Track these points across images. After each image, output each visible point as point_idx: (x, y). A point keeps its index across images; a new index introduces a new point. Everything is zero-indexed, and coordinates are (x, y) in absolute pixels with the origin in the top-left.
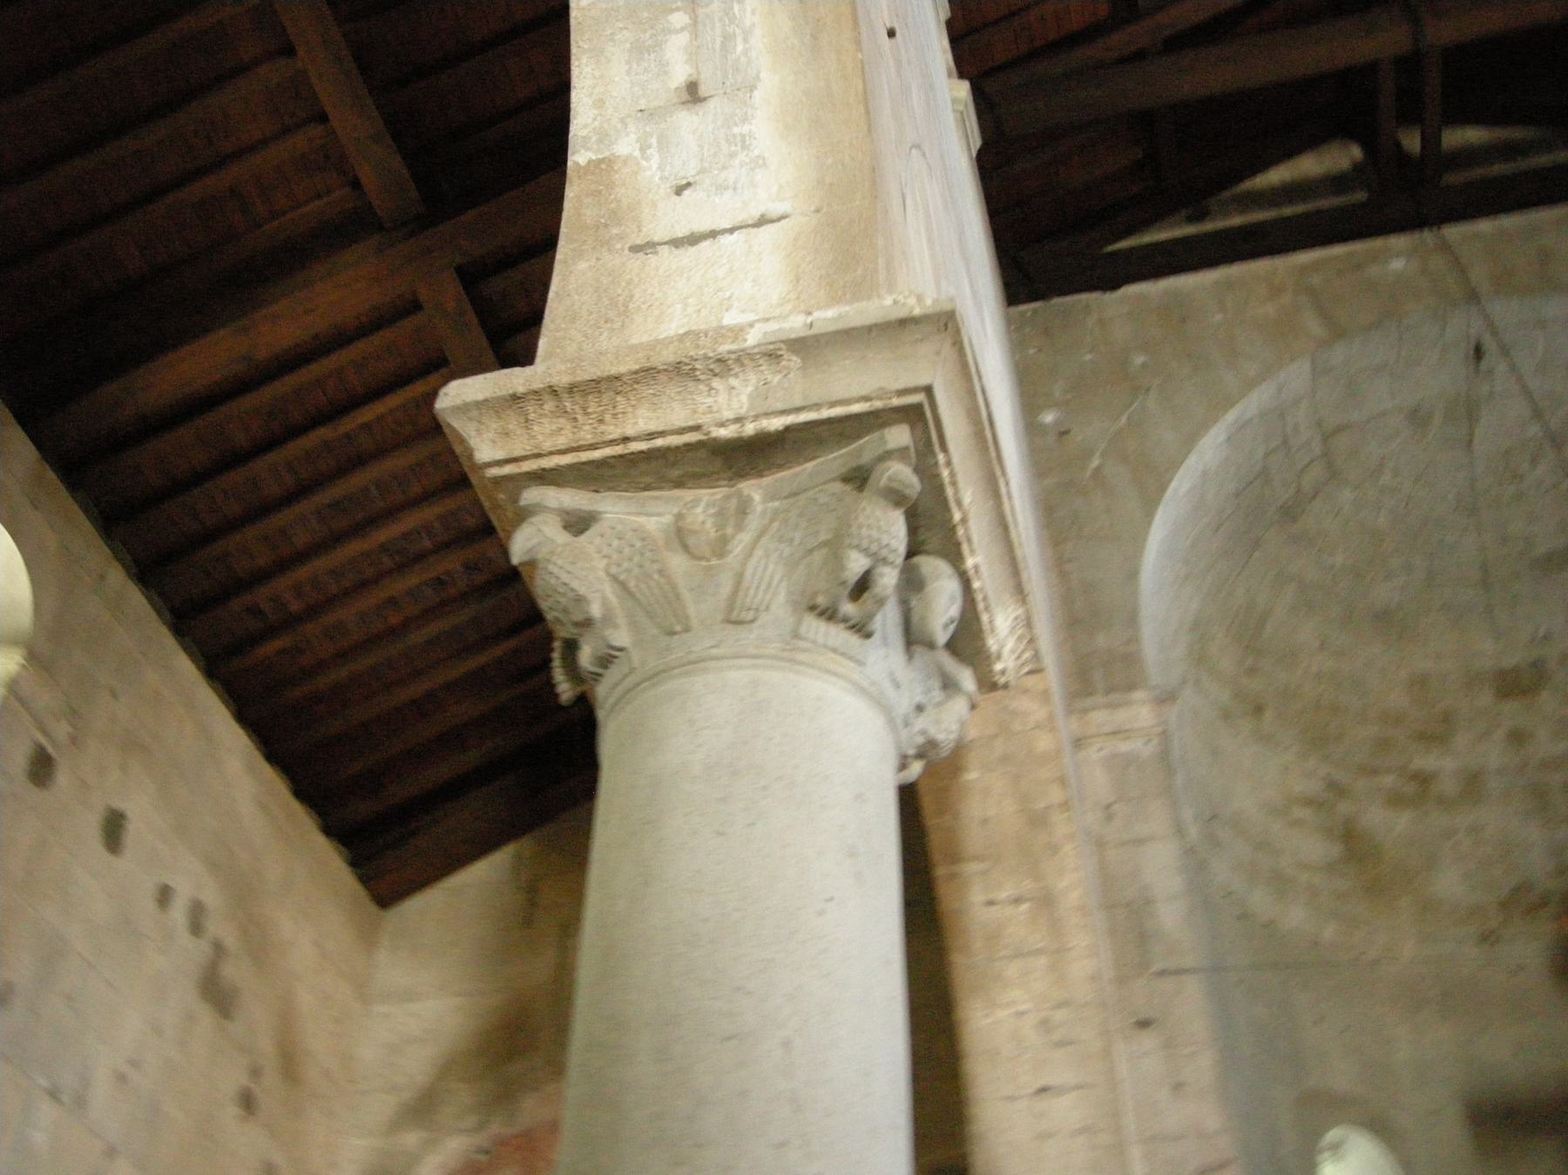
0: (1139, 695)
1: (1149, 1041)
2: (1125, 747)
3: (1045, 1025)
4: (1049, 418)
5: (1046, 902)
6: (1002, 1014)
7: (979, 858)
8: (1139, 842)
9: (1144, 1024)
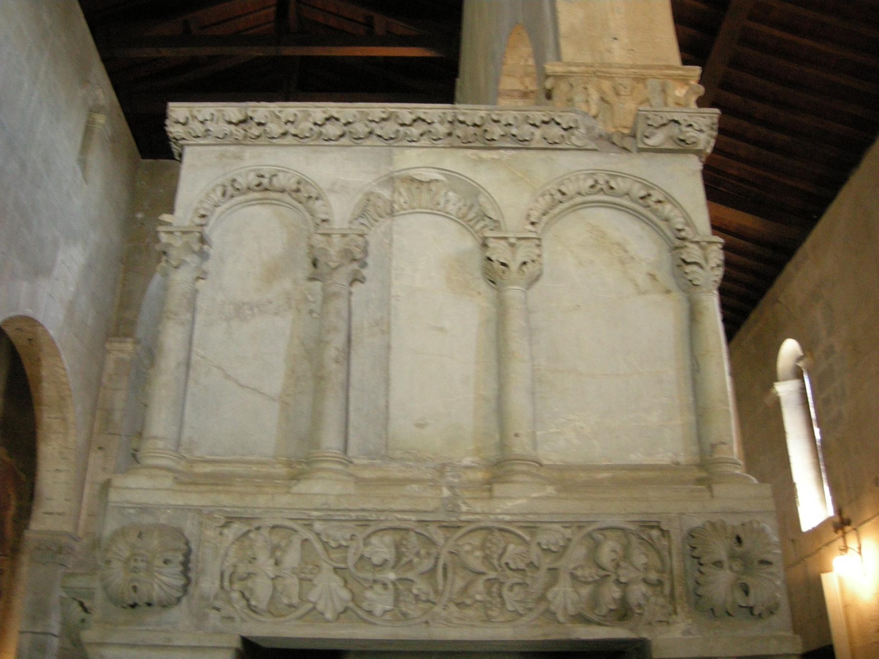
0: (129, 340)
1: (100, 454)
2: (122, 355)
3: (61, 453)
4: (140, 216)
5: (64, 420)
6: (50, 448)
7: (46, 406)
8: (115, 390)
9: (101, 448)
